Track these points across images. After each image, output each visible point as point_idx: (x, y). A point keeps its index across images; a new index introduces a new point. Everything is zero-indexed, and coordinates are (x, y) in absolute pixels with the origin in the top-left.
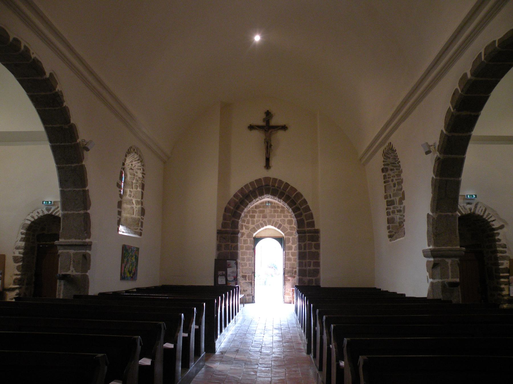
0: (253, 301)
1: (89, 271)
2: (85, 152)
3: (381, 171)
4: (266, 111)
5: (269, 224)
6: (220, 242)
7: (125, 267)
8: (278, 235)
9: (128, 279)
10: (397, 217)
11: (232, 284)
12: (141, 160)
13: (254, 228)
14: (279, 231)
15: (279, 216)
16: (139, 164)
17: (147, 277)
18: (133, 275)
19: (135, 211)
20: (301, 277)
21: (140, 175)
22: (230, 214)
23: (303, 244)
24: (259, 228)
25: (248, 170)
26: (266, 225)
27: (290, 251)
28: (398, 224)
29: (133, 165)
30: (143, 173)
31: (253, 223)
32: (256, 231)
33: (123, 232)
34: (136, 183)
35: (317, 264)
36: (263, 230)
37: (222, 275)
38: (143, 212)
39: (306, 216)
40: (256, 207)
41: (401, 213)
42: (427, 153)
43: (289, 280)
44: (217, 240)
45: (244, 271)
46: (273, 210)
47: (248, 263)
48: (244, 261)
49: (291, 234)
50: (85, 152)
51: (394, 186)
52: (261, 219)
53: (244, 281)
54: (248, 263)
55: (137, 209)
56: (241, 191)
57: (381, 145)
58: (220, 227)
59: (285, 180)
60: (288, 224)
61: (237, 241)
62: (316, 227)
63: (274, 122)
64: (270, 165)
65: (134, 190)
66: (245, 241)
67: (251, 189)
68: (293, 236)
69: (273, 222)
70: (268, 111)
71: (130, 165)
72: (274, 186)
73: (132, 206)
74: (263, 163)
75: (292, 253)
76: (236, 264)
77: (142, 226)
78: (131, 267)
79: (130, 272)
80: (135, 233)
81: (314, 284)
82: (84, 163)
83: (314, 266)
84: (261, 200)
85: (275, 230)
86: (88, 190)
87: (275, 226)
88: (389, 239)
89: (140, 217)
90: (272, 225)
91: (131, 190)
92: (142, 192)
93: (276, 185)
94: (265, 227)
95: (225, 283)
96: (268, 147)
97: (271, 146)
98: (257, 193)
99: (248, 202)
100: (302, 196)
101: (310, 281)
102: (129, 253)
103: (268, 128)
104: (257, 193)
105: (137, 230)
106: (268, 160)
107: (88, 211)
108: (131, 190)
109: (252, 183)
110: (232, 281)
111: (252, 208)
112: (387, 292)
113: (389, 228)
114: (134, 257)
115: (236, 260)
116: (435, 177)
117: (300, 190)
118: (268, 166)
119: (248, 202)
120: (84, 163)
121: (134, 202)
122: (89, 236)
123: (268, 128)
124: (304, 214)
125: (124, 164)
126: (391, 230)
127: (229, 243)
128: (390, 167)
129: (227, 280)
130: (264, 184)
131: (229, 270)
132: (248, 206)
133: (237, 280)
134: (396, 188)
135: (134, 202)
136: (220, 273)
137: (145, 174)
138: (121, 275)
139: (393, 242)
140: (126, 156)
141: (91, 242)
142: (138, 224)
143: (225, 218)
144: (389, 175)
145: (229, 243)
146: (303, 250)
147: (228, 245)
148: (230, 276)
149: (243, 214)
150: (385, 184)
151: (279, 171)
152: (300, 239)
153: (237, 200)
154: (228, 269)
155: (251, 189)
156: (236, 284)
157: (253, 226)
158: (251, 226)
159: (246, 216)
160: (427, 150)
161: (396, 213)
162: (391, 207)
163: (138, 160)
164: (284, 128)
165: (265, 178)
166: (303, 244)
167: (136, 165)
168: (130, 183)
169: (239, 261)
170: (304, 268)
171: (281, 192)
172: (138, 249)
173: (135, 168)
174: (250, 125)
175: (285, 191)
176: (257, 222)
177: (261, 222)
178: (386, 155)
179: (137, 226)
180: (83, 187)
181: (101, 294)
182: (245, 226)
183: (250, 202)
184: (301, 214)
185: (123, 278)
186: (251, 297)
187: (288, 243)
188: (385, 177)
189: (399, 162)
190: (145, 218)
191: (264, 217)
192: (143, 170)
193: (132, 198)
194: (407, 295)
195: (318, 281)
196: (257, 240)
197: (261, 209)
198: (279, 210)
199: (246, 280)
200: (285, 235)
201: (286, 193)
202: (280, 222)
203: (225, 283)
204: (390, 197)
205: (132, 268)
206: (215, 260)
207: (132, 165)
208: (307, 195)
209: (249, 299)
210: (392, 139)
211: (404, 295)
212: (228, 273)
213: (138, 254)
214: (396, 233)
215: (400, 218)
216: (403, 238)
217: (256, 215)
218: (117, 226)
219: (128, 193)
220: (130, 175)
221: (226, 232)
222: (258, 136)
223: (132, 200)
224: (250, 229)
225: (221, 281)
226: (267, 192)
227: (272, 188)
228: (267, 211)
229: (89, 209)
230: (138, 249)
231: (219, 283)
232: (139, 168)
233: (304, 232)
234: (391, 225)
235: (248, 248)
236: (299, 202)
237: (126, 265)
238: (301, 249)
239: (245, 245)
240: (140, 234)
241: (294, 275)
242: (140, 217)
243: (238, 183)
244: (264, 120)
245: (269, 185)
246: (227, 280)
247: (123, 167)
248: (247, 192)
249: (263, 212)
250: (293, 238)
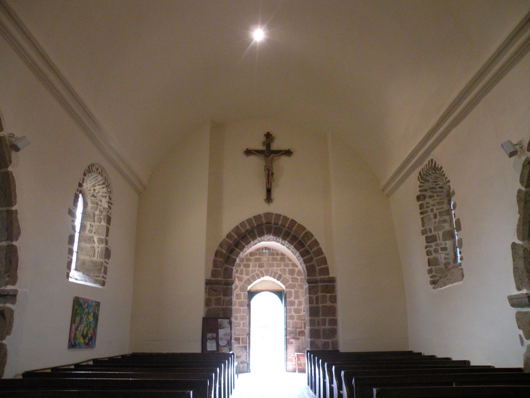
0: (248, 370)
1: (8, 337)
2: (14, 154)
3: (416, 199)
4: (266, 133)
5: (267, 275)
6: (209, 295)
7: (77, 329)
8: (276, 288)
9: (80, 347)
10: (442, 256)
11: (225, 350)
12: (107, 184)
13: (249, 280)
14: (279, 283)
15: (278, 266)
16: (105, 190)
17: (110, 343)
18: (89, 340)
19: (96, 252)
20: (312, 339)
21: (106, 205)
22: (222, 260)
23: (314, 297)
24: (255, 280)
25: (245, 204)
26: (263, 276)
27: (292, 307)
28: (443, 266)
29: (97, 191)
30: (109, 202)
31: (247, 274)
32: (251, 283)
33: (77, 279)
34: (100, 215)
35: (334, 322)
36: (259, 283)
37: (213, 338)
38: (107, 253)
39: (317, 260)
40: (251, 254)
41: (447, 252)
42: (512, 155)
43: (292, 343)
44: (206, 292)
45: (237, 333)
46: (271, 257)
47: (241, 322)
48: (237, 320)
49: (293, 287)
50: (14, 154)
51: (435, 217)
52: (257, 268)
53: (238, 345)
54: (241, 322)
55: (99, 249)
56: (237, 229)
57: (413, 168)
58: (209, 277)
59: (291, 216)
60: (289, 274)
61: (231, 294)
62: (331, 275)
63: (275, 146)
64: (272, 198)
65: (97, 224)
66: (238, 296)
67: (248, 227)
68: (296, 289)
69: (272, 273)
70: (268, 133)
71: (92, 191)
72: (277, 224)
73: (93, 245)
74: (264, 195)
75: (294, 309)
76: (230, 323)
77: (105, 272)
78: (86, 329)
79: (84, 337)
80: (96, 282)
81: (330, 349)
82: (10, 169)
83: (330, 325)
84: (260, 242)
85: (274, 282)
86: (16, 211)
87: (274, 277)
88: (431, 287)
89: (103, 261)
90: (270, 276)
91: (92, 223)
92: (108, 229)
93: (280, 223)
94: (262, 279)
95: (215, 349)
96: (270, 175)
97: (273, 174)
98: (256, 233)
99: (244, 244)
100: (312, 236)
101: (326, 344)
102: (84, 310)
103: (269, 152)
104: (256, 233)
105: (98, 278)
106: (269, 191)
107: (15, 243)
108: (92, 223)
109: (249, 221)
110: (225, 346)
111: (247, 255)
112: (433, 357)
113: (430, 271)
114: (92, 314)
115: (229, 319)
116: (523, 189)
117: (309, 228)
118: (269, 199)
119: (244, 244)
120: (10, 169)
121: (96, 240)
122: (14, 282)
123: (269, 152)
124: (315, 259)
125: (80, 185)
126: (433, 274)
127: (221, 297)
128: (428, 193)
129: (218, 345)
130: (264, 221)
131: (221, 332)
132: (245, 249)
133: (231, 345)
134: (437, 220)
135: (96, 240)
136: (209, 335)
137: (112, 204)
138: (70, 340)
139: (440, 289)
140: (85, 175)
141: (16, 291)
142: (101, 269)
143: (215, 264)
144: (427, 203)
145: (221, 297)
146: (314, 305)
147: (220, 299)
148: (222, 339)
149: (238, 261)
150: (422, 216)
151: (283, 206)
152: (311, 290)
153: (231, 242)
154: (220, 330)
155: (248, 227)
156: (230, 350)
157: (248, 277)
158: (245, 277)
159: (239, 265)
160: (512, 150)
161: (440, 252)
162: (433, 244)
163: (103, 184)
164: (288, 153)
165: (267, 213)
166: (314, 297)
167: (100, 190)
168: (91, 214)
169: (233, 320)
170: (316, 327)
171: (286, 232)
172: (98, 304)
173: (98, 194)
174: (247, 149)
175: (291, 229)
176: (252, 272)
177: (257, 272)
178: (422, 177)
179: (97, 270)
180: (8, 206)
181: (28, 375)
182: (237, 277)
183: (247, 244)
184: (311, 259)
185: (73, 345)
186: (246, 365)
187: (290, 298)
188: (421, 206)
189: (449, 181)
190: (110, 261)
191: (261, 266)
192: (110, 198)
193: (93, 234)
194: (475, 362)
195: (335, 344)
196: (251, 294)
197: (256, 257)
198: (279, 257)
199: (239, 343)
200: (286, 288)
201: (293, 233)
202: (279, 273)
203: (215, 349)
204: (431, 231)
205: (88, 331)
206: (204, 318)
207: (94, 190)
208: (319, 236)
209: (244, 369)
210: (435, 155)
211: (468, 362)
212: (220, 335)
213: (98, 310)
214: (441, 278)
215: (445, 258)
216: (461, 282)
217: (251, 264)
218: (67, 270)
219: (88, 227)
220: (92, 203)
221: (218, 283)
222: (256, 163)
223: (93, 237)
224: (244, 280)
225: (211, 346)
226: (269, 232)
227: (274, 226)
228: (264, 259)
229: (17, 240)
230: (98, 304)
231: (208, 349)
232: (104, 195)
233: (316, 282)
234: (433, 267)
235: (241, 304)
236: (308, 243)
237: (78, 327)
238: (313, 304)
239: (238, 301)
240: (103, 284)
241: (297, 336)
242: (103, 261)
243: (233, 219)
244: (264, 143)
245: (270, 223)
246: (218, 345)
247: (80, 189)
248: (243, 231)
249: (258, 260)
250: (295, 291)
